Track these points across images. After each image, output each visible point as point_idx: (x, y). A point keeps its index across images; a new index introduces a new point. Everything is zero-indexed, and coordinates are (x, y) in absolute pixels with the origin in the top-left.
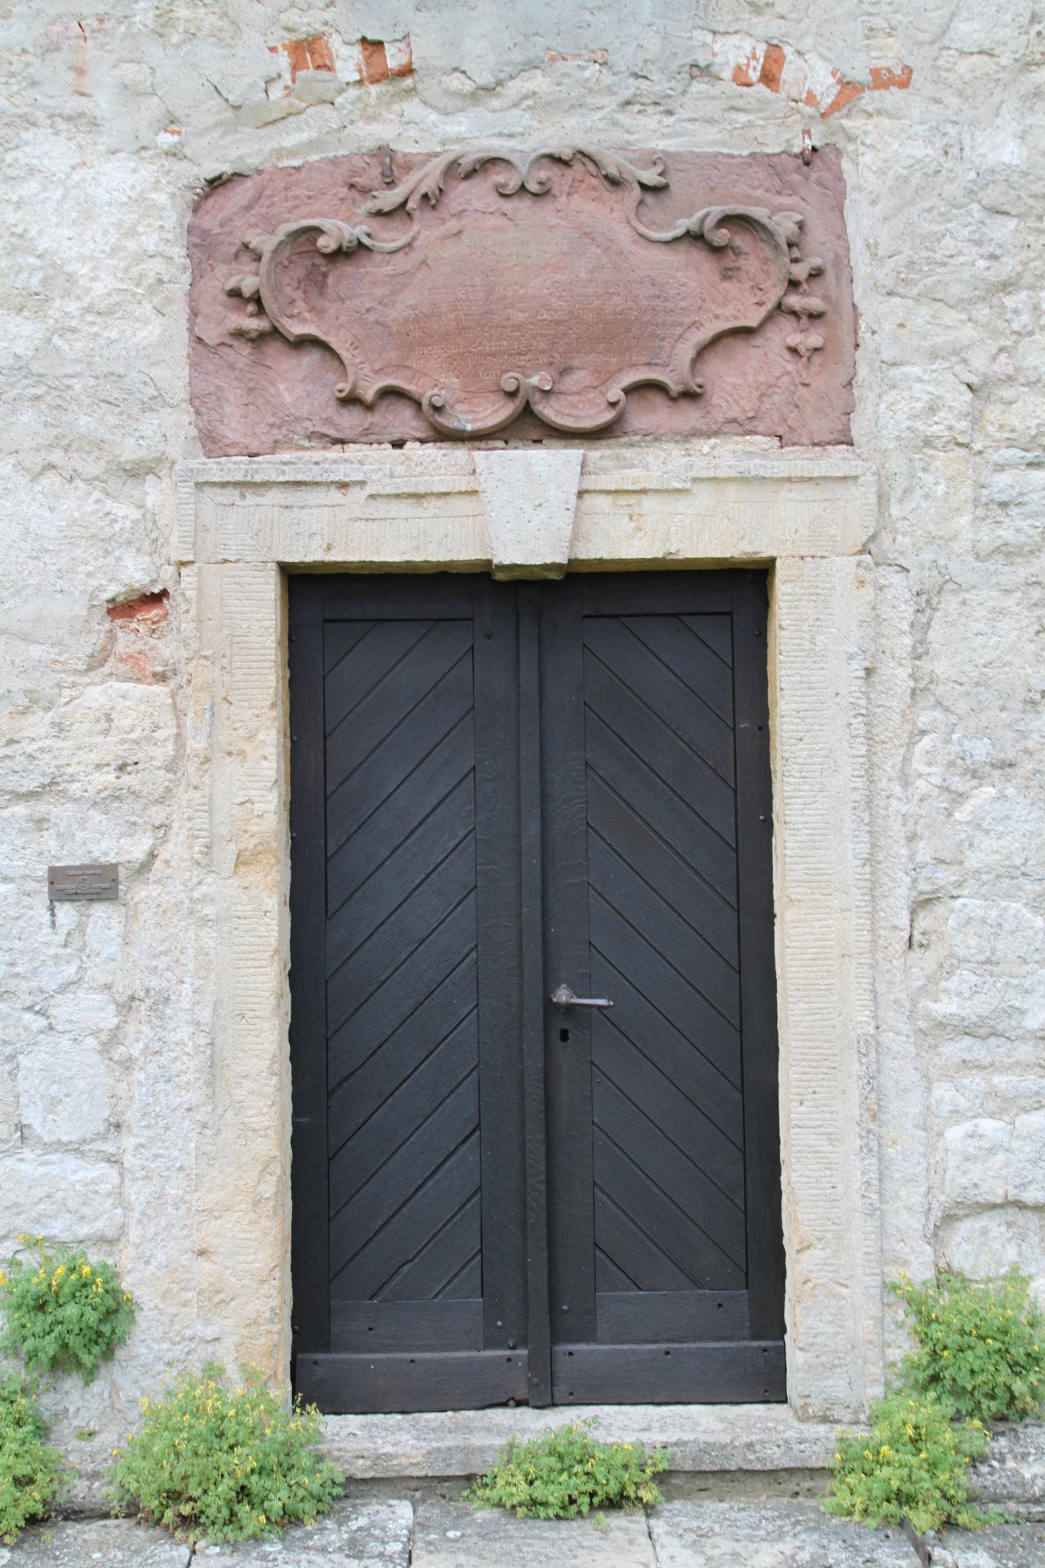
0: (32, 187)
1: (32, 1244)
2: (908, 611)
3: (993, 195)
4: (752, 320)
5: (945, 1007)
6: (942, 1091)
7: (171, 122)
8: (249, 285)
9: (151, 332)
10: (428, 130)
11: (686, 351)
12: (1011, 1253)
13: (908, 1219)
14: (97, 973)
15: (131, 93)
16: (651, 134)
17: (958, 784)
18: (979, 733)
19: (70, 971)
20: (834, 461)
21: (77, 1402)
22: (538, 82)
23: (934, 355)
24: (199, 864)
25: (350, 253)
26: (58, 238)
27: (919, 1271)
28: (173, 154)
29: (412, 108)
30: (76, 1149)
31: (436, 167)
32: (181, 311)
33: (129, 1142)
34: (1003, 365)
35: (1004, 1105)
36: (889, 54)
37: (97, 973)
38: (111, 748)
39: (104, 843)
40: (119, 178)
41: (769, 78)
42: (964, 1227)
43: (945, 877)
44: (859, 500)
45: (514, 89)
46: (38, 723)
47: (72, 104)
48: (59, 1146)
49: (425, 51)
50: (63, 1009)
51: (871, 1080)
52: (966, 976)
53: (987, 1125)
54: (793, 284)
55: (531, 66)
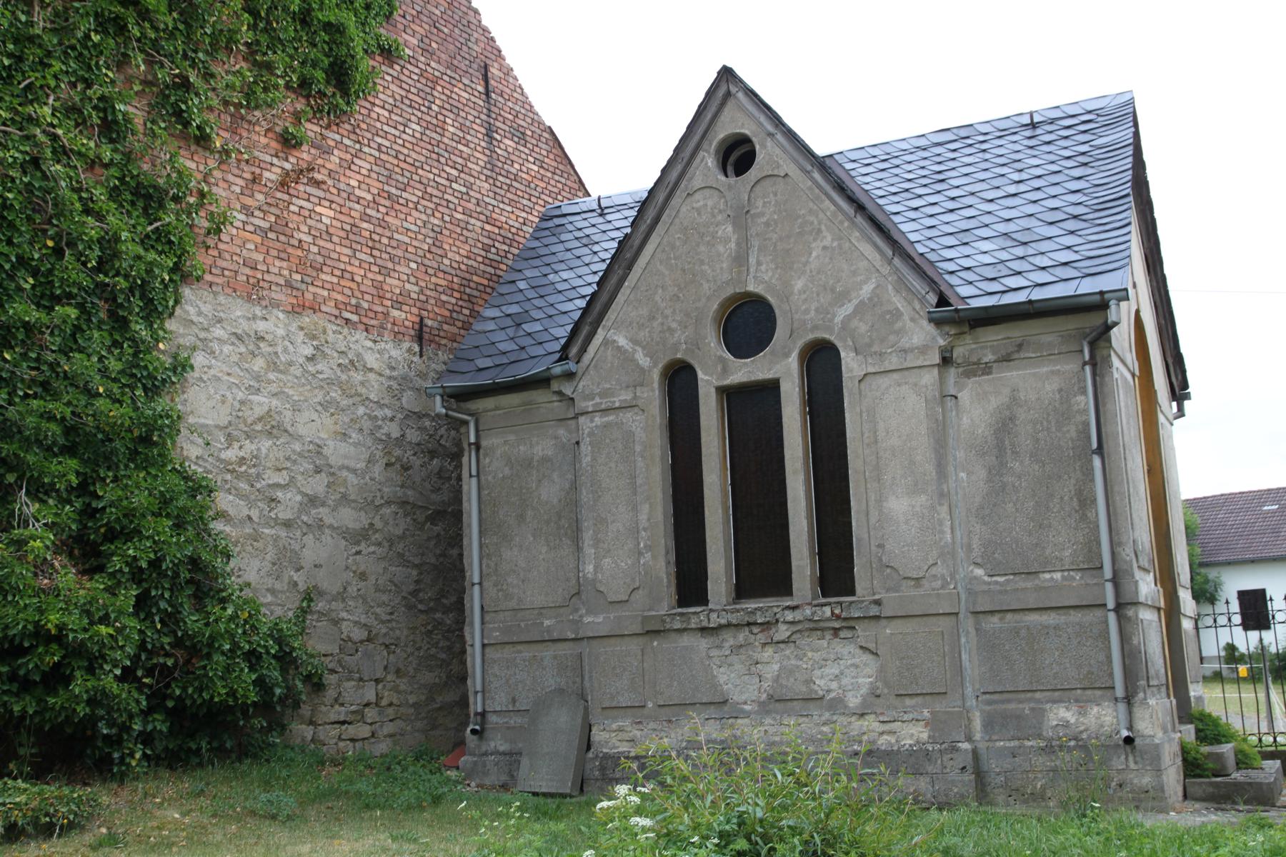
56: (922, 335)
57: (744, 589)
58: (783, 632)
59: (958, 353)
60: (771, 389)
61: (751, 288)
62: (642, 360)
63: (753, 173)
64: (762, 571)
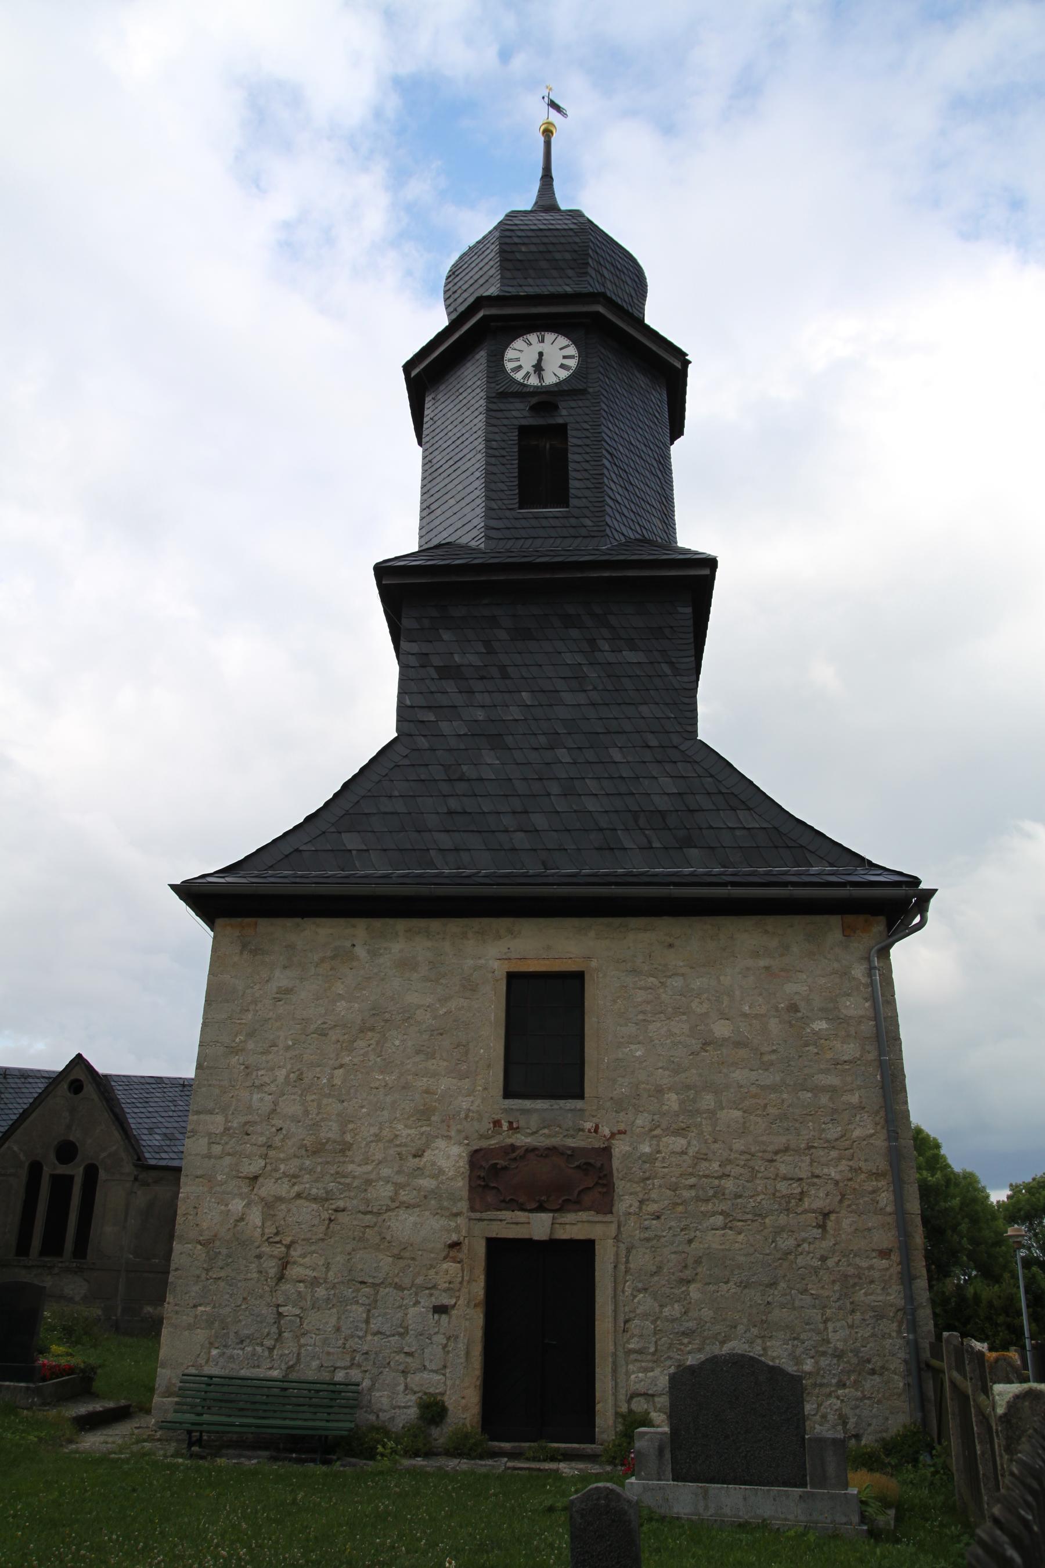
0: (436, 1152)
1: (425, 1394)
2: (624, 1252)
3: (644, 1158)
4: (591, 1186)
5: (631, 1346)
6: (631, 1367)
7: (467, 1138)
8: (482, 1174)
9: (460, 1184)
10: (522, 1140)
11: (576, 1192)
12: (646, 1406)
13: (622, 1397)
14: (442, 1331)
15: (459, 1131)
16: (571, 1142)
17: (635, 1293)
18: (640, 1281)
19: (436, 1330)
20: (608, 1218)
21: (435, 1432)
22: (546, 1131)
23: (631, 1194)
24: (328, 1163)
25: (505, 1168)
26: (443, 1163)
27: (624, 1409)
28: (468, 1145)
29: (518, 1136)
30: (435, 1372)
31: (523, 1149)
32: (467, 1179)
33: (448, 1371)
34: (646, 1196)
35: (645, 1370)
36: (622, 1127)
37: (442, 1331)
38: (448, 1278)
39: (446, 1301)
40: (455, 1150)
41: (596, 1131)
42: (635, 1400)
43: (632, 1315)
44: (613, 1228)
45: (541, 1132)
46: (432, 1272)
47: (446, 1134)
48: (432, 1371)
49: (522, 1123)
50: (435, 1338)
51: (614, 1363)
52: (636, 1339)
53: (640, 1375)
54: (600, 1178)
55: (545, 1127)
56: (128, 1168)
57: (43, 1252)
58: (56, 1270)
59: (141, 1177)
60: (71, 1178)
61: (71, 1139)
62: (22, 1157)
63: (81, 1095)
64: (53, 1246)
